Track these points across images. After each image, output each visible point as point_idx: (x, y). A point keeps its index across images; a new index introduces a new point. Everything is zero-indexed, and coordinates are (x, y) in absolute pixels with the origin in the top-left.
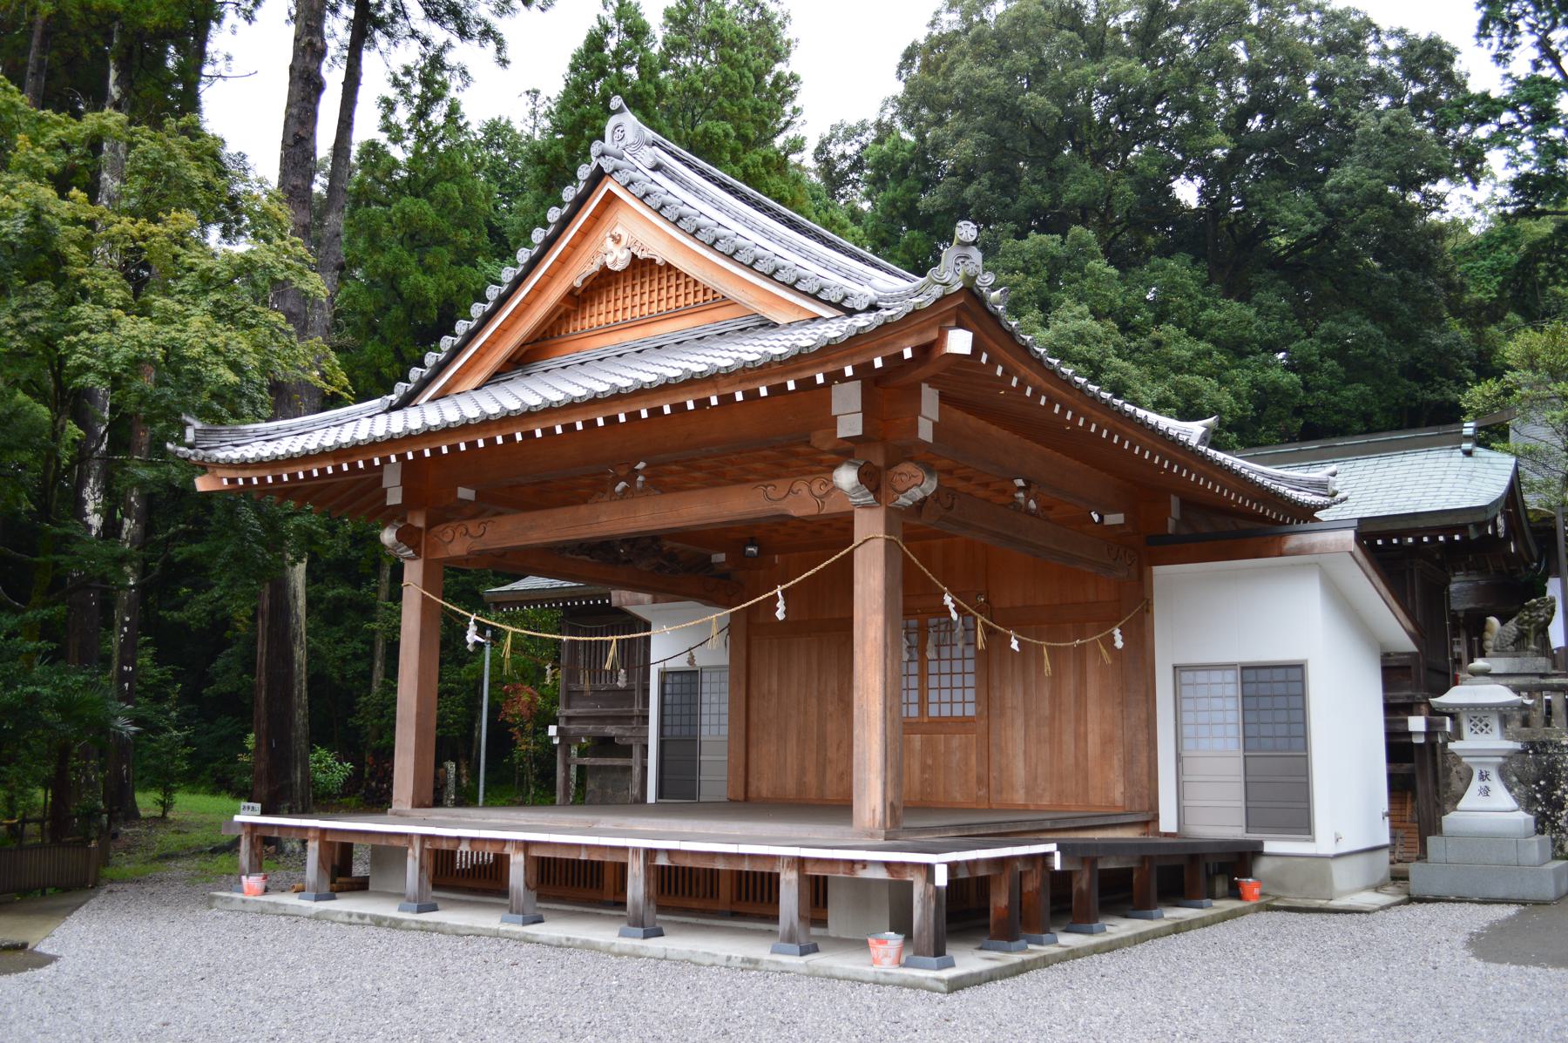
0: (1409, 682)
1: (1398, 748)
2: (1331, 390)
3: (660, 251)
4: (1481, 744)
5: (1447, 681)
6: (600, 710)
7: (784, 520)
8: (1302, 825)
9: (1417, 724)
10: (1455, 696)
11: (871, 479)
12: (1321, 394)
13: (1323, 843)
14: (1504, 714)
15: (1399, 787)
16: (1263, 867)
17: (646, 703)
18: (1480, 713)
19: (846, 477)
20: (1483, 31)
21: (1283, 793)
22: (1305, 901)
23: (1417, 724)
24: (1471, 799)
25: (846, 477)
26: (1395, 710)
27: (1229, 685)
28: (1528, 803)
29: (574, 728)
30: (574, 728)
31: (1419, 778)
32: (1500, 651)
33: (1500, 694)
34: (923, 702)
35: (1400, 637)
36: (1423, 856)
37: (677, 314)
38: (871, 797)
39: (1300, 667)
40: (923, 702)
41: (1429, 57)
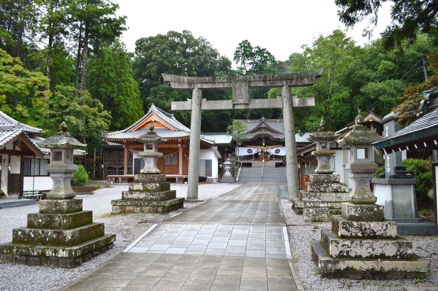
0: (221, 161)
1: (219, 168)
2: (209, 113)
3: (158, 121)
4: (227, 168)
5: (224, 161)
6: (110, 163)
7: (172, 148)
8: (211, 175)
9: (221, 166)
10: (225, 163)
11: (181, 145)
12: (207, 114)
13: (213, 177)
14: (230, 165)
15: (219, 172)
16: (207, 180)
17: (132, 162)
18: (227, 165)
19: (180, 145)
20: (235, 59)
21: (209, 173)
22: (211, 182)
23: (221, 166)
24: (226, 173)
25: (180, 145)
26: (219, 164)
27: (204, 162)
28: (231, 174)
29: (106, 165)
30: (106, 165)
31: (221, 171)
32: (230, 158)
33: (229, 163)
34: (171, 163)
35: (220, 156)
36: (221, 179)
37: (159, 126)
38: (181, 172)
39: (211, 160)
40: (171, 163)
41: (226, 63)
